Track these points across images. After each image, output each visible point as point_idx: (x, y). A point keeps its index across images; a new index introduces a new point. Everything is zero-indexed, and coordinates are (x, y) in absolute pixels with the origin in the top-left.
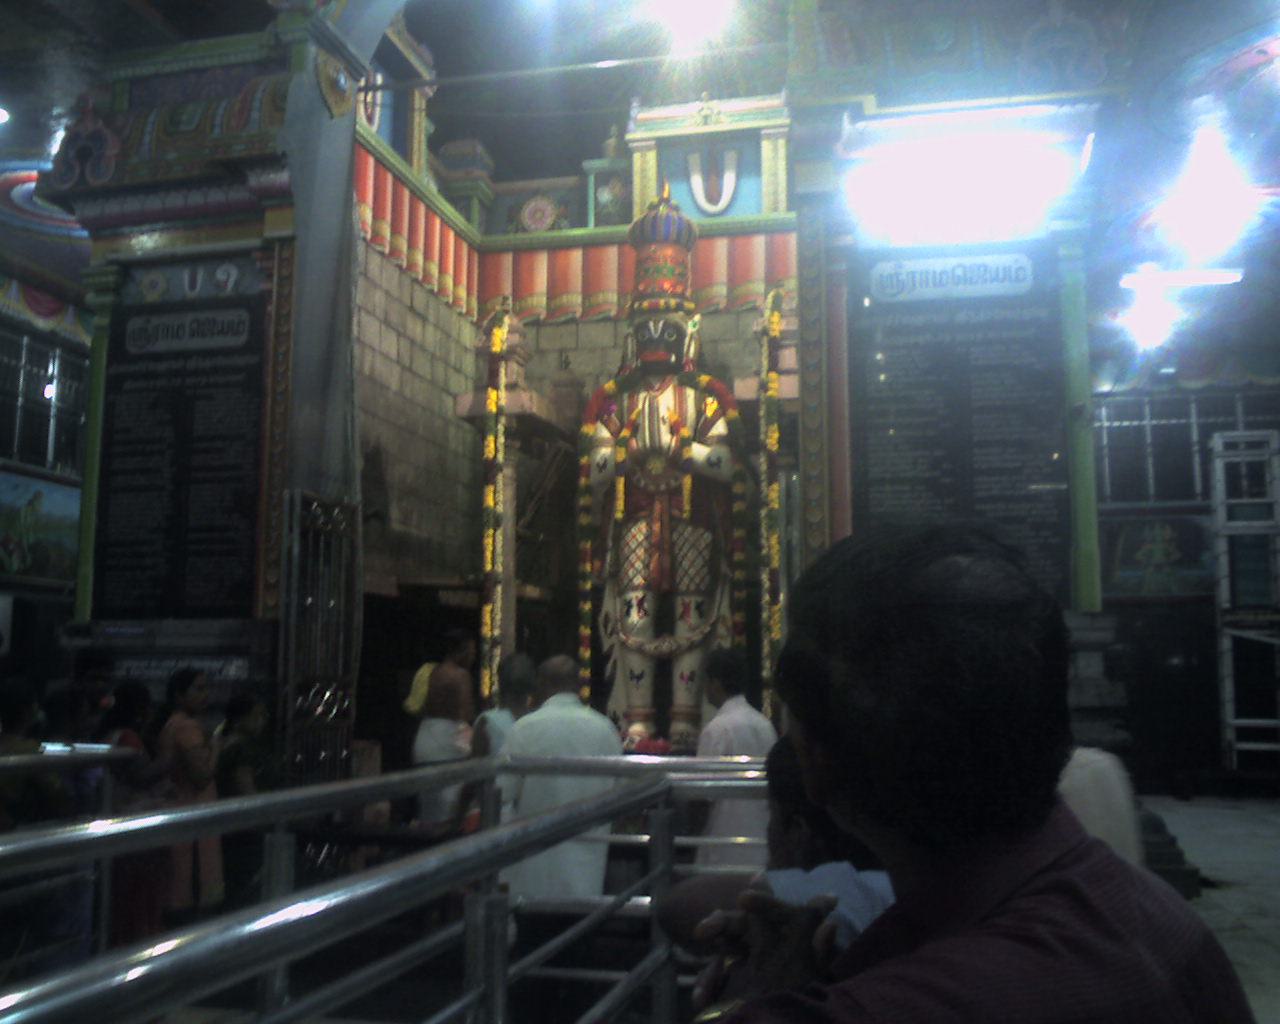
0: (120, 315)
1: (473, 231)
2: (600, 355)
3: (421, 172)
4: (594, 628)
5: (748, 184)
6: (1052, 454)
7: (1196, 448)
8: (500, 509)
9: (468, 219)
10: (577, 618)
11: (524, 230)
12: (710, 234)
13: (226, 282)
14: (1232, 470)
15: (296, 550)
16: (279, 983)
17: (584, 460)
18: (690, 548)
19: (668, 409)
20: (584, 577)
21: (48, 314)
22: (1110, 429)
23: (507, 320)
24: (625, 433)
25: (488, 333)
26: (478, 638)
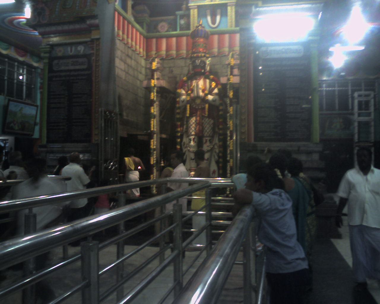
0: (52, 59)
1: (144, 32)
2: (182, 68)
3: (130, 16)
4: (181, 146)
5: (224, 19)
6: (309, 96)
7: (350, 96)
8: (155, 113)
9: (143, 28)
10: (176, 144)
11: (159, 32)
12: (213, 34)
13: (80, 50)
14: (360, 103)
15: (103, 125)
16: (122, 228)
17: (178, 100)
18: (208, 124)
19: (202, 86)
20: (178, 132)
21: (22, 56)
22: (326, 90)
23: (156, 60)
24: (189, 92)
25: (151, 63)
26: (150, 149)
